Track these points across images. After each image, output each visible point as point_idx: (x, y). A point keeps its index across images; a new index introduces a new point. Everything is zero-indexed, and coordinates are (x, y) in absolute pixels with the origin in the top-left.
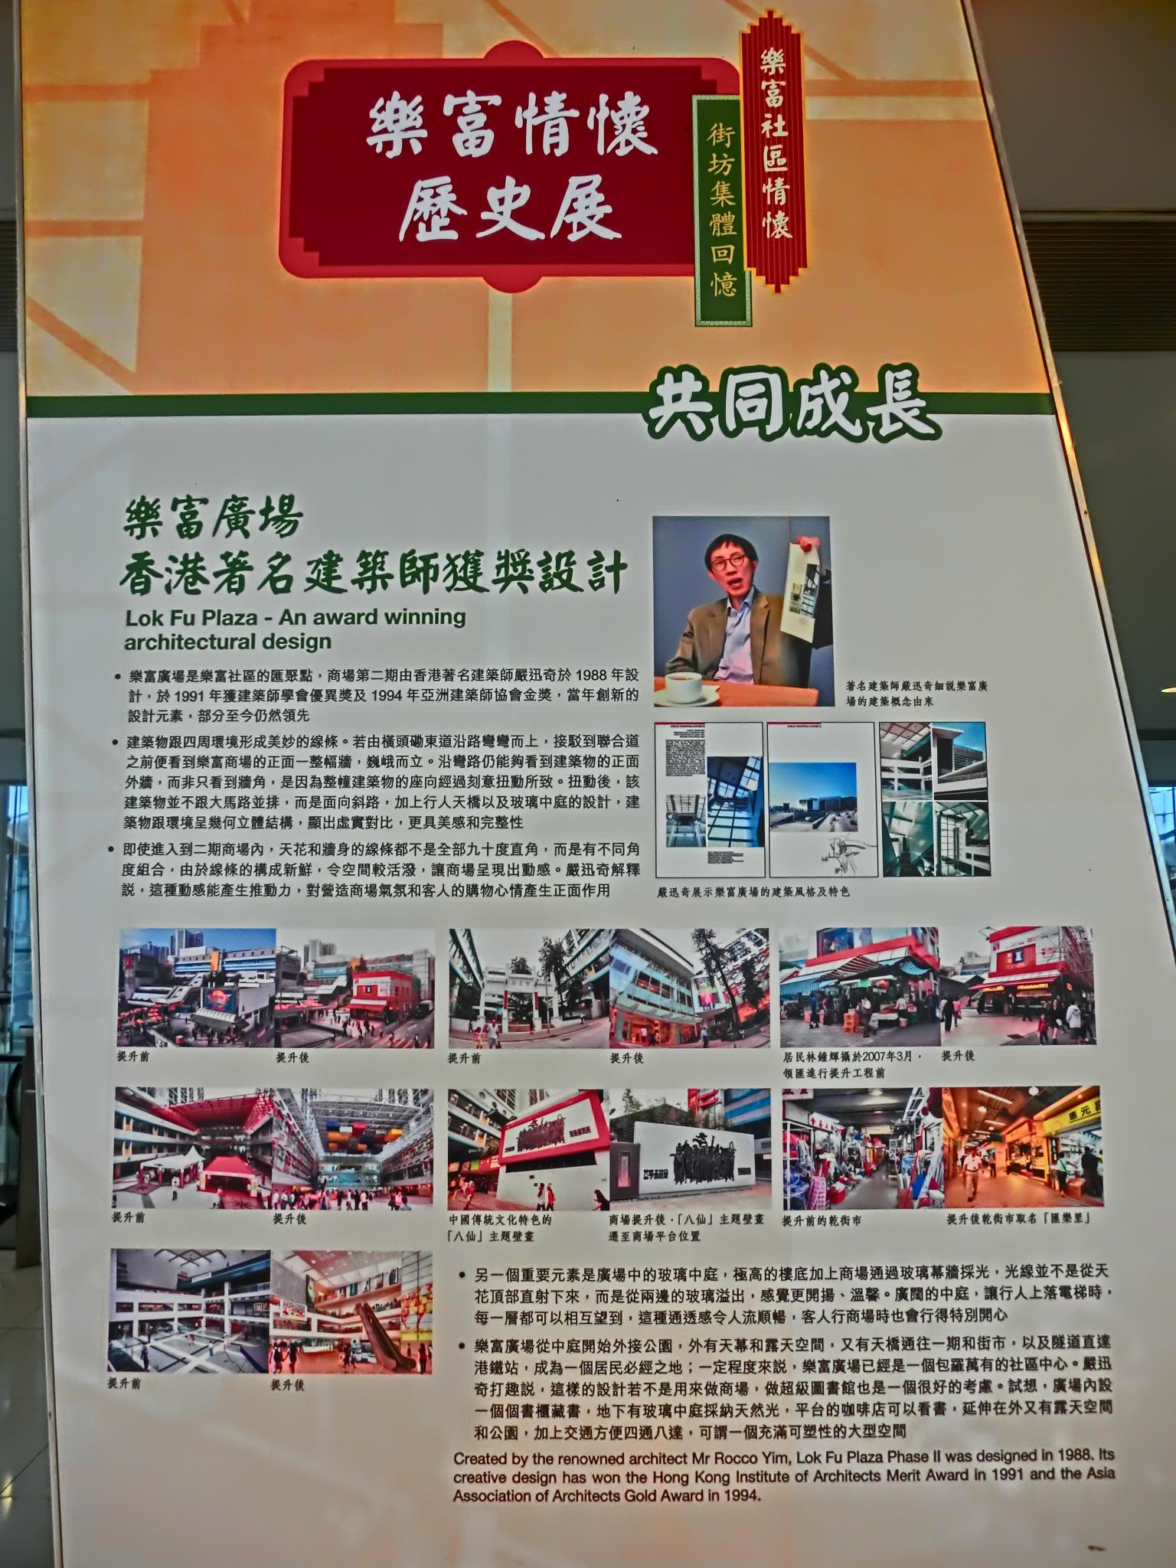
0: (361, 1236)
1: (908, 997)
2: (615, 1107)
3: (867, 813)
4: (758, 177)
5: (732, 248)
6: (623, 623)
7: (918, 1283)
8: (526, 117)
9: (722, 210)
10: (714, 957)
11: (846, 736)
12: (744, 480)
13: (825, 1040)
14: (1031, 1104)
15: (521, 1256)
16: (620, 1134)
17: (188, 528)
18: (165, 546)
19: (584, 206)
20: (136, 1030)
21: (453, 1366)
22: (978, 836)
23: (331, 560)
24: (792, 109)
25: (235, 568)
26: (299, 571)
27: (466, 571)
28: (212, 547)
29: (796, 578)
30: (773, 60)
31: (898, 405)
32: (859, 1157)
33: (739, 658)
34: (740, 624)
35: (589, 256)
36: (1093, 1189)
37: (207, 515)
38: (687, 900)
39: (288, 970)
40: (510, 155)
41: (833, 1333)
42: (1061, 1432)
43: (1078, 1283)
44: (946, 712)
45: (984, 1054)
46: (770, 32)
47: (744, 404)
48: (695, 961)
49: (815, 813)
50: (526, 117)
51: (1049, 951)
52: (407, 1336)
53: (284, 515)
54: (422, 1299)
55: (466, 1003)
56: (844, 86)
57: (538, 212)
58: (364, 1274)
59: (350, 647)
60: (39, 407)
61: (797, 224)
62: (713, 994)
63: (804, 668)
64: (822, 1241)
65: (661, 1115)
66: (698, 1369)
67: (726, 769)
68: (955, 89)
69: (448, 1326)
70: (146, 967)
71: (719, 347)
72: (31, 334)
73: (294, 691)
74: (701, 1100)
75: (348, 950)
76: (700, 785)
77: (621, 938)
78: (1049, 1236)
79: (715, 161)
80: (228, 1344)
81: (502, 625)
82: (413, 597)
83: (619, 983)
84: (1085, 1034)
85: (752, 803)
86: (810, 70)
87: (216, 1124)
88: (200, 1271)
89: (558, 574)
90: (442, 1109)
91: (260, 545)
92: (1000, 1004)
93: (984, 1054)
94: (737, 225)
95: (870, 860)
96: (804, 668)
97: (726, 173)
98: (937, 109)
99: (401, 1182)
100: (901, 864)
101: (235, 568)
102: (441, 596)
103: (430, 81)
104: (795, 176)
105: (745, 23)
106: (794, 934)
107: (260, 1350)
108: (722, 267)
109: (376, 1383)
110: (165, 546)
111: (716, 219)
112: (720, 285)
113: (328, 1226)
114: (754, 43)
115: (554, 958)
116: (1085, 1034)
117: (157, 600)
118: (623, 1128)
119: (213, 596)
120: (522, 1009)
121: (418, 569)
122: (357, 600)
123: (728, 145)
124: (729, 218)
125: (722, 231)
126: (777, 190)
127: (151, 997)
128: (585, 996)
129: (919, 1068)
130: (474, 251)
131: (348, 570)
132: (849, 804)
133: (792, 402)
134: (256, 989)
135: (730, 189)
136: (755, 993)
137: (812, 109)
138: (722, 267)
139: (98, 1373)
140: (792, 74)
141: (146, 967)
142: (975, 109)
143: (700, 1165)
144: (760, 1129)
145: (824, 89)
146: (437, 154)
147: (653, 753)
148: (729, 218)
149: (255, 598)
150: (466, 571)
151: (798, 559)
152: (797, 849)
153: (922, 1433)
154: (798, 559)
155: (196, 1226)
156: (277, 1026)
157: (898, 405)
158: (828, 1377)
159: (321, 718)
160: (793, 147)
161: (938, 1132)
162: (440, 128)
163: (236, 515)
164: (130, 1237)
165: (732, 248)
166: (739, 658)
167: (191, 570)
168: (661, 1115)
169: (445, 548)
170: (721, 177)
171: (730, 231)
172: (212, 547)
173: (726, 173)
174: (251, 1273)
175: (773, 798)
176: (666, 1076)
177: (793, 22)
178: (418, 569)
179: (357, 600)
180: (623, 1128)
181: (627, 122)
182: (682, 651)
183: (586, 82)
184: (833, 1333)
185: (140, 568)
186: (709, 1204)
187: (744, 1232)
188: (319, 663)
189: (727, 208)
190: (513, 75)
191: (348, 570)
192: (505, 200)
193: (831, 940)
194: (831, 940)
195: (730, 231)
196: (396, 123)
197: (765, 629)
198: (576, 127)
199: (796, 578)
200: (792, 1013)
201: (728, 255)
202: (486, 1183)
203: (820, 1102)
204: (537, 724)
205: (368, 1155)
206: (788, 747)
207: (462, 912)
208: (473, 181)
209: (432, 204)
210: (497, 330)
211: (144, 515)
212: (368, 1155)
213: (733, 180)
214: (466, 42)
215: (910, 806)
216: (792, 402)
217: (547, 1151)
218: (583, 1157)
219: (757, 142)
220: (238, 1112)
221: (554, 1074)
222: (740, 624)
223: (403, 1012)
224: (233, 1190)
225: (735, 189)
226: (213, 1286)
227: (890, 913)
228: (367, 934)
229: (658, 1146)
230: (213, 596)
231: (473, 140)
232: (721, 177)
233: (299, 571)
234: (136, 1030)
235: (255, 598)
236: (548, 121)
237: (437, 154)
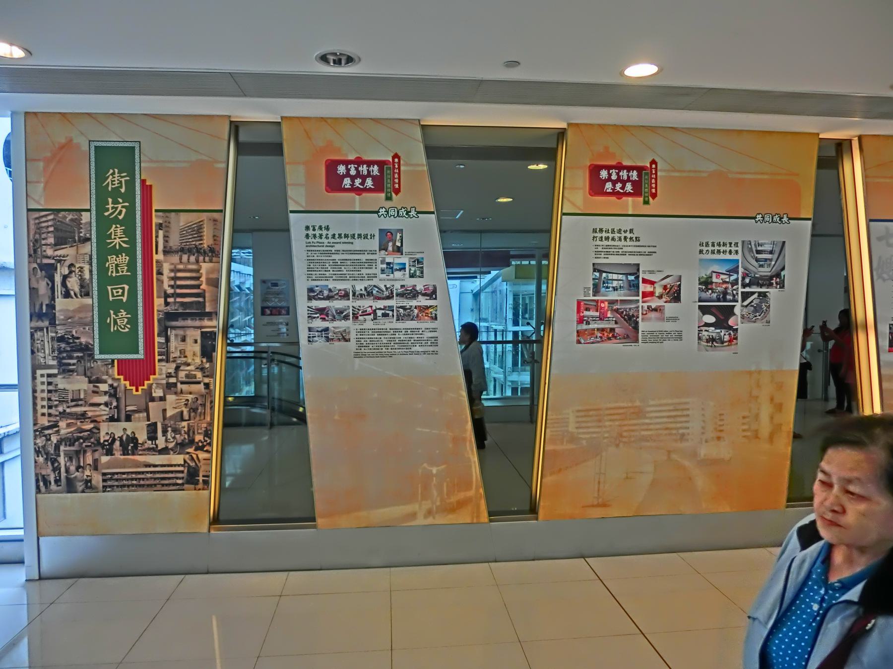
0: (341, 324)
1: (413, 294)
2: (374, 308)
3: (407, 269)
4: (394, 178)
5: (127, 287)
6: (375, 244)
7: (413, 330)
8: (360, 169)
9: (117, 252)
10: (387, 289)
11: (405, 260)
12: (390, 224)
13: (401, 299)
14: (427, 308)
15: (362, 327)
16: (374, 312)
17: (314, 230)
18: (311, 232)
19: (369, 183)
20: (310, 298)
21: (353, 341)
22: (422, 272)
23: (334, 235)
24: (399, 168)
25: (321, 236)
26: (330, 236)
27: (353, 236)
28: (317, 233)
29: (398, 237)
30: (396, 160)
31: (413, 213)
32: (406, 314)
33: (390, 248)
34: (390, 244)
35: (369, 190)
36: (436, 318)
37: (317, 228)
38: (382, 282)
39: (330, 290)
40: (358, 175)
41: (402, 337)
42: (431, 349)
43: (434, 330)
44: (418, 256)
45: (423, 301)
46: (396, 156)
47: (392, 213)
48: (384, 289)
49: (400, 270)
50: (360, 169)
51: (431, 288)
52: (347, 337)
53: (327, 228)
54: (349, 333)
55: (354, 295)
56: (407, 164)
57: (362, 183)
58: (341, 330)
59: (338, 247)
60: (292, 212)
61: (399, 186)
62: (386, 293)
63: (399, 250)
64: (400, 325)
65: (380, 309)
66: (385, 341)
67: (388, 264)
68: (422, 165)
69: (353, 336)
70: (311, 290)
71: (388, 204)
72: (290, 201)
73: (329, 253)
74: (385, 307)
75: (339, 287)
76: (385, 266)
77: (375, 286)
78: (431, 325)
79: (110, 206)
80: (324, 339)
81: (358, 244)
82: (345, 240)
83: (374, 292)
84: (436, 299)
85: (392, 268)
86: (402, 162)
87: (321, 311)
88: (320, 329)
89: (366, 237)
90: (351, 308)
91: (324, 232)
92: (424, 295)
93: (423, 301)
94: (132, 265)
95: (408, 276)
96: (399, 250)
97: (121, 217)
98: (420, 168)
99: (346, 318)
100: (412, 276)
101: (321, 236)
102: (350, 240)
103: (346, 163)
104: (399, 178)
105: (392, 154)
106: (397, 285)
107: (328, 339)
108: (117, 306)
109: (343, 343)
110: (311, 232)
111: (112, 260)
112: (115, 322)
113: (337, 324)
114: (394, 158)
115: (366, 289)
116: (436, 299)
117: (310, 240)
118: (375, 311)
119: (318, 240)
120: (361, 295)
121: (346, 236)
122: (338, 240)
123: (123, 190)
124: (124, 259)
125: (117, 271)
126: (397, 181)
127: (312, 294)
128: (370, 294)
129: (414, 303)
130: (353, 189)
131: (337, 236)
132: (404, 269)
133: (398, 212)
134: (326, 293)
135: (125, 232)
136: (392, 293)
137: (402, 168)
138: (117, 306)
139: (306, 342)
140: (399, 163)
141: (311, 290)
142: (425, 168)
143: (385, 315)
144: (393, 311)
145: (404, 165)
146: (348, 175)
147: (379, 262)
148: (124, 259)
149: (324, 240)
150: (353, 236)
151: (399, 235)
152: (398, 274)
153: (414, 349)
154: (399, 235)
155: (319, 324)
156: (329, 298)
157: (413, 213)
158: (401, 342)
159: (334, 257)
160: (399, 174)
161: (416, 311)
162: (348, 170)
163: (320, 228)
164: (311, 325)
165: (127, 287)
166: (390, 248)
167: (315, 236)
168: (380, 309)
169: (350, 233)
170: (116, 221)
171: (124, 271)
172: (317, 233)
173: (121, 217)
174: (327, 329)
175: (395, 267)
176: (381, 304)
177: (400, 154)
178: (346, 236)
179: (338, 240)
180: (375, 311)
181: (375, 170)
182: (383, 247)
183: (370, 163)
184: (402, 337)
185: (307, 236)
186: (386, 320)
187: (391, 324)
188: (333, 249)
189: (122, 250)
190: (359, 162)
191: (337, 236)
192: (358, 182)
193: (402, 286)
194: (402, 286)
195: (124, 271)
196: (342, 169)
197: (394, 244)
198: (368, 170)
199: (398, 237)
200: (397, 295)
201: (123, 295)
202: (357, 318)
203: (401, 307)
204: (363, 257)
205: (341, 314)
206: (397, 261)
207: (354, 283)
208: (353, 178)
209: (347, 182)
210: (357, 202)
211: (307, 228)
212: (341, 314)
213: (128, 224)
214: (352, 157)
215: (413, 269)
216: (398, 212)
217: (365, 313)
218: (370, 314)
219: (394, 173)
220: (324, 309)
221: (366, 304)
222: (390, 244)
223: (346, 296)
224: (324, 319)
225: (130, 232)
226: (321, 331)
227: (409, 282)
228: (341, 286)
229: (379, 313)
230: (318, 240)
231: (353, 172)
232: (116, 221)
233: (330, 236)
234: (310, 298)
235: (324, 240)
236: (364, 169)
237: (348, 175)
